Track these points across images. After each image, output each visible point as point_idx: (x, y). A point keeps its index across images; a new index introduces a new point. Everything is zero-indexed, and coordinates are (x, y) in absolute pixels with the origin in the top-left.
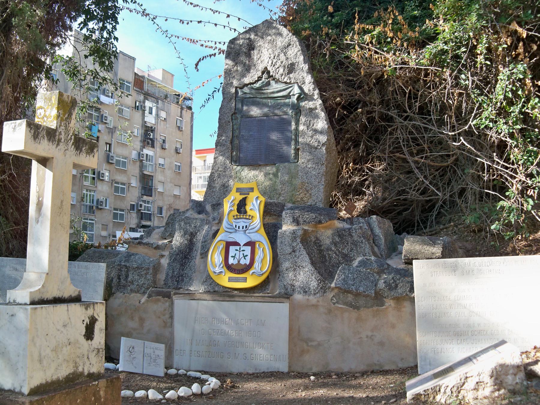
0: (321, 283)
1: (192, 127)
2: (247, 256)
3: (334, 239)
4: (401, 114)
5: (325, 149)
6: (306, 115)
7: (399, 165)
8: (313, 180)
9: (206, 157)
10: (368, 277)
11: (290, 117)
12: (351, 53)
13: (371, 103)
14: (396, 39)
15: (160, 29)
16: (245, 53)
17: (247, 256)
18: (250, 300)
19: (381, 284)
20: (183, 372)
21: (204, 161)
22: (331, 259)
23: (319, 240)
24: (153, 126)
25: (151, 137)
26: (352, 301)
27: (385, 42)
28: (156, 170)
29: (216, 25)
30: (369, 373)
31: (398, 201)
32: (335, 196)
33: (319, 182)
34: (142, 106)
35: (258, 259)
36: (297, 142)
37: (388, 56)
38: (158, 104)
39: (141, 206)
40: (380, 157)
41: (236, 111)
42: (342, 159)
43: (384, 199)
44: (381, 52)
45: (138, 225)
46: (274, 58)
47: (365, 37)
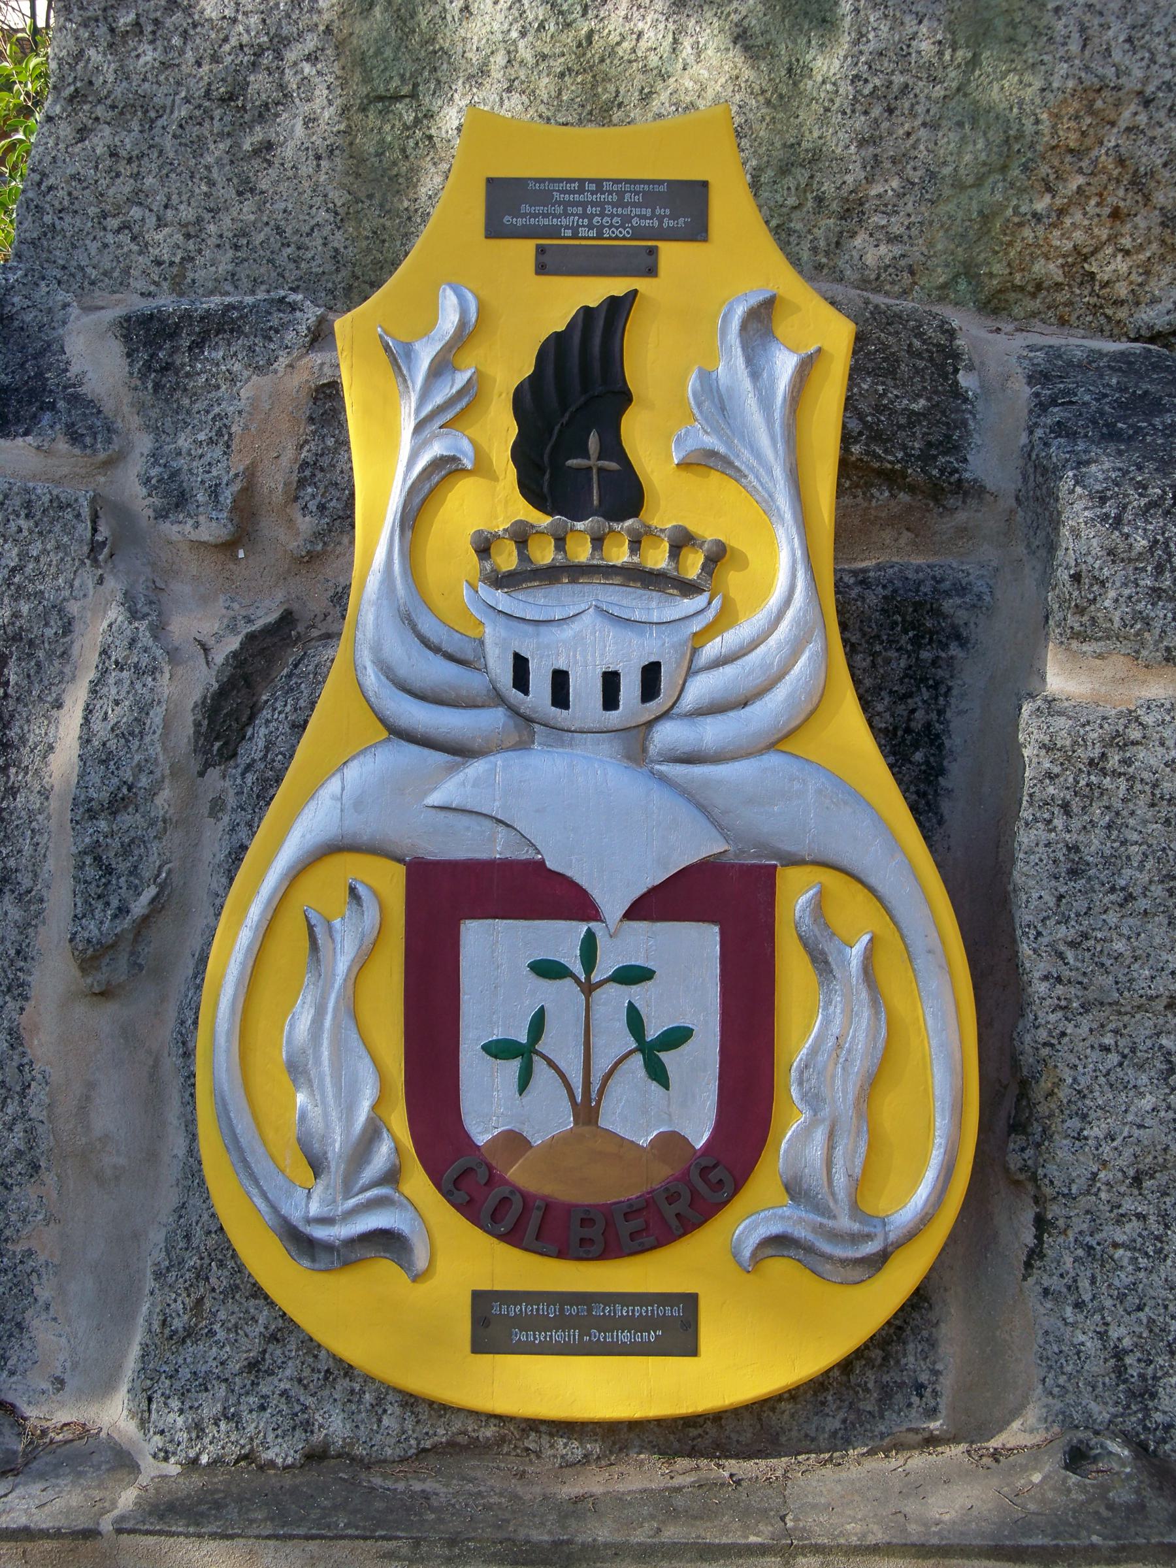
2: (677, 1037)
17: (677, 1037)
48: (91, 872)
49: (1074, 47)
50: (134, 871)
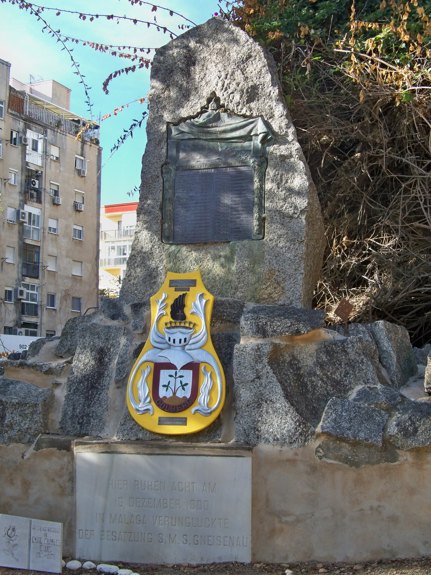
0: (299, 425)
1: (99, 179)
2: (186, 384)
3: (319, 358)
4: (421, 160)
5: (306, 219)
6: (276, 167)
7: (419, 240)
8: (287, 267)
9: (121, 216)
10: (372, 416)
11: (250, 169)
12: (344, 66)
13: (375, 144)
14: (414, 45)
15: (48, 28)
16: (182, 70)
17: (186, 384)
18: (192, 453)
19: (392, 429)
20: (91, 565)
21: (119, 222)
22: (315, 389)
23: (296, 360)
24: (38, 169)
25: (37, 186)
26: (348, 453)
27: (396, 49)
28: (44, 237)
29: (135, 21)
30: (375, 565)
31: (417, 294)
32: (320, 287)
33: (296, 270)
34: (21, 138)
35: (203, 390)
36: (262, 208)
37: (401, 72)
38: (46, 136)
39: (22, 293)
40: (389, 226)
41: (169, 161)
42: (332, 230)
43: (396, 292)
44: (391, 66)
45: (17, 322)
46: (226, 78)
47: (366, 42)
48: (118, 371)
49: (268, 264)
50: (124, 371)
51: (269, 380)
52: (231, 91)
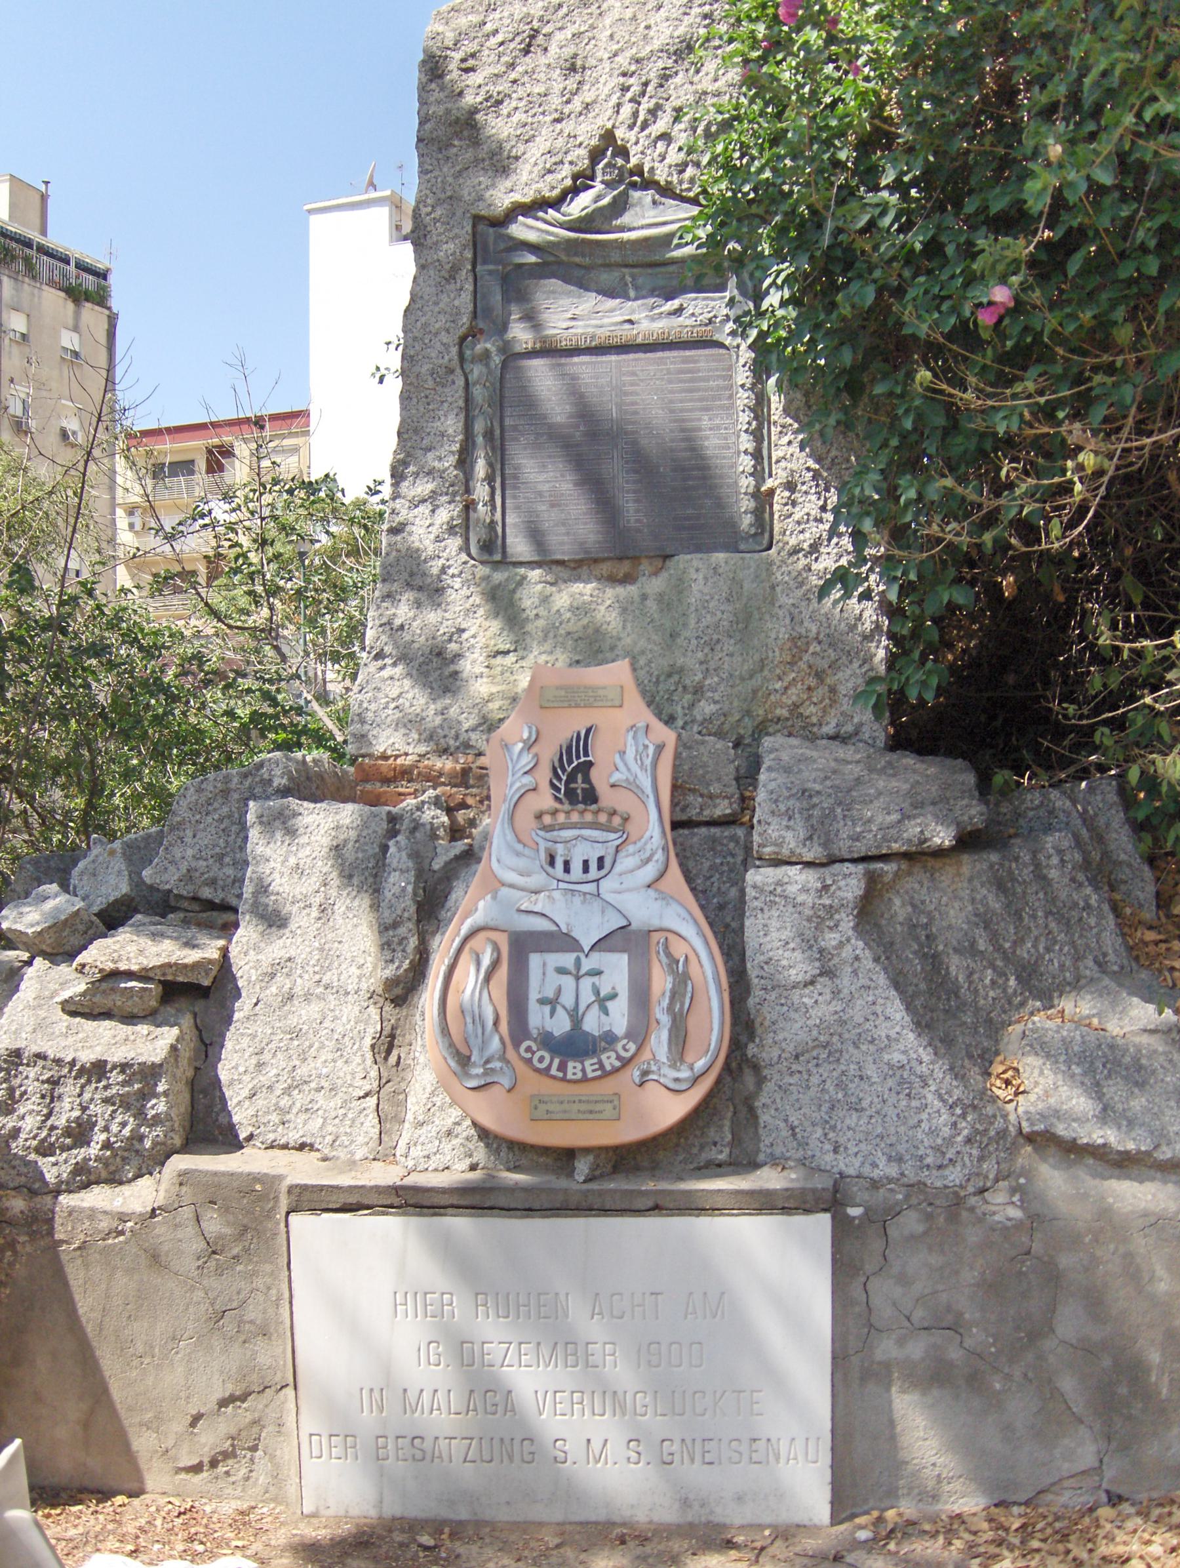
0: (963, 1116)
2: (613, 996)
46: (643, 94)
51: (862, 982)
52: (662, 130)
